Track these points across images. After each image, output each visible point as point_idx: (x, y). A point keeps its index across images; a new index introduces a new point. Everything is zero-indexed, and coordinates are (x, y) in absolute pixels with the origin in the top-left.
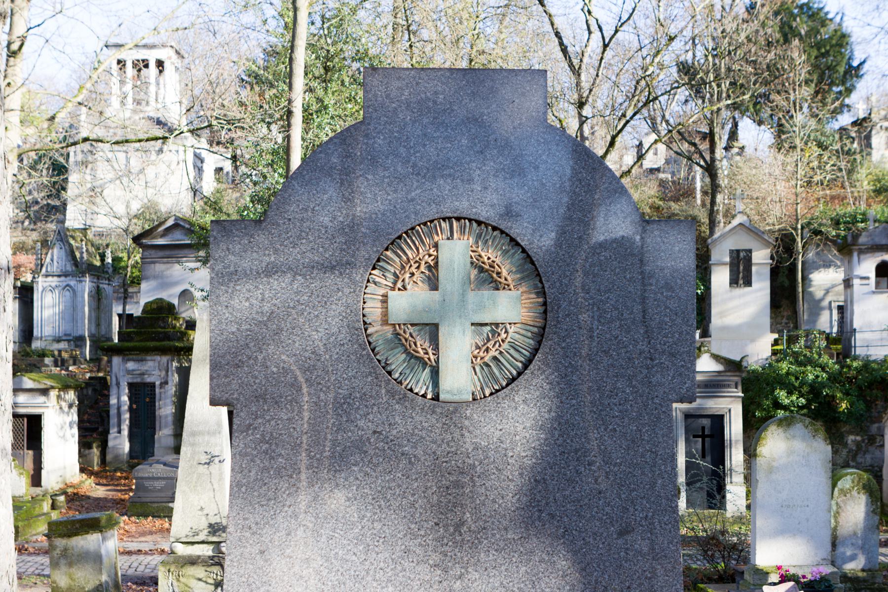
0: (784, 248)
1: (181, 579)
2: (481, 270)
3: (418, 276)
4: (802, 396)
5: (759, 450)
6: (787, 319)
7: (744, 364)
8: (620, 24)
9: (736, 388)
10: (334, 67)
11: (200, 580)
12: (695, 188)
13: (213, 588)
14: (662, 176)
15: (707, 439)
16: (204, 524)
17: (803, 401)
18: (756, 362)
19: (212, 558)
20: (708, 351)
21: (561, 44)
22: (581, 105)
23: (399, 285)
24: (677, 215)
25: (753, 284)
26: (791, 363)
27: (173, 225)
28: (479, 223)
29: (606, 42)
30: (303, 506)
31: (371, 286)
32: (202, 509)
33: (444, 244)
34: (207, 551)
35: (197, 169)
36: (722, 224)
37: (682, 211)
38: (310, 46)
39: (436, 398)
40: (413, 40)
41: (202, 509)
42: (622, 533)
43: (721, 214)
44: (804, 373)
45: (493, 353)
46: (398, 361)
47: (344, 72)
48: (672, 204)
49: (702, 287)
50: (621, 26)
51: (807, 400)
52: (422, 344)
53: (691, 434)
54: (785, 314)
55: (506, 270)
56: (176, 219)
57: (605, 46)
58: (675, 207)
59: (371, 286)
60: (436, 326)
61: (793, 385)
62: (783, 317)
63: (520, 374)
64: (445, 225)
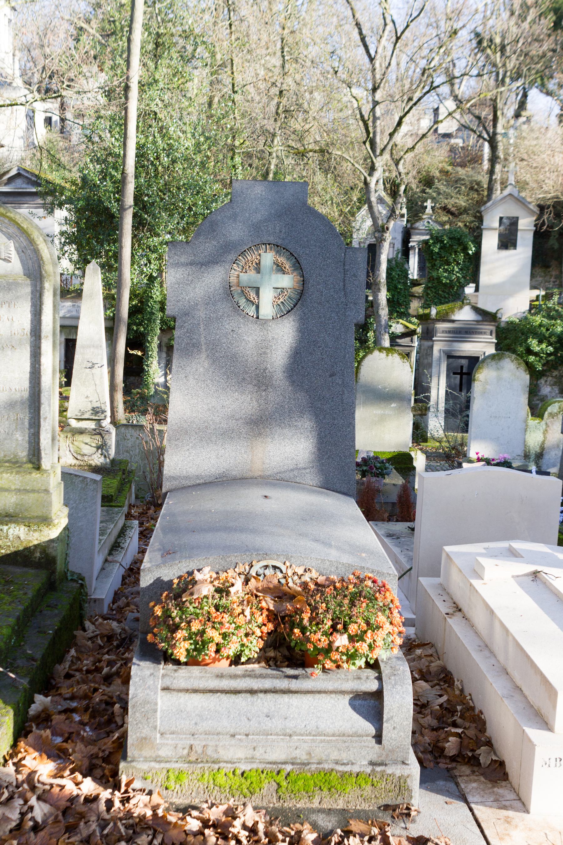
0: (555, 214)
1: (75, 443)
2: (278, 266)
3: (252, 268)
4: (550, 344)
5: (477, 376)
6: (555, 278)
7: (499, 315)
8: (411, 19)
9: (491, 335)
10: (163, 43)
11: (86, 444)
12: (482, 155)
13: (95, 449)
14: (453, 141)
15: (464, 376)
16: (90, 407)
17: (551, 349)
18: (515, 315)
19: (95, 430)
20: (469, 304)
21: (361, 33)
22: (375, 89)
23: (244, 271)
24: (463, 179)
25: (518, 248)
26: (544, 317)
27: (16, 174)
28: (278, 246)
29: (399, 35)
30: (203, 359)
31: (233, 271)
32: (87, 397)
33: (263, 254)
34: (91, 425)
35: (28, 118)
36: (499, 192)
37: (468, 177)
38: (146, 27)
39: (258, 318)
40: (232, 19)
41: (87, 397)
42: (331, 376)
43: (499, 182)
44: (554, 325)
45: (281, 300)
46: (242, 302)
47: (173, 50)
48: (459, 169)
49: (474, 249)
50: (412, 21)
51: (555, 348)
52: (253, 295)
53: (451, 372)
54: (554, 273)
55: (287, 266)
56: (18, 170)
57: (398, 38)
58: (461, 172)
59: (233, 271)
60: (258, 288)
61: (544, 335)
62: (551, 276)
63: (292, 309)
64: (264, 247)
